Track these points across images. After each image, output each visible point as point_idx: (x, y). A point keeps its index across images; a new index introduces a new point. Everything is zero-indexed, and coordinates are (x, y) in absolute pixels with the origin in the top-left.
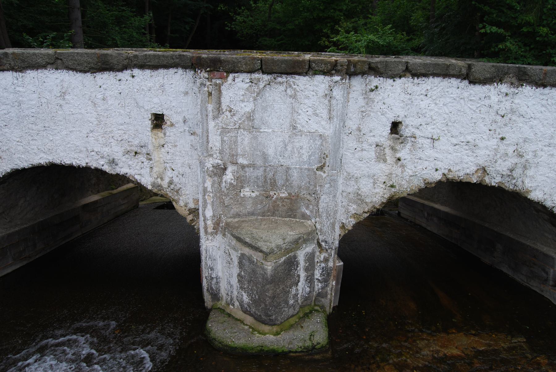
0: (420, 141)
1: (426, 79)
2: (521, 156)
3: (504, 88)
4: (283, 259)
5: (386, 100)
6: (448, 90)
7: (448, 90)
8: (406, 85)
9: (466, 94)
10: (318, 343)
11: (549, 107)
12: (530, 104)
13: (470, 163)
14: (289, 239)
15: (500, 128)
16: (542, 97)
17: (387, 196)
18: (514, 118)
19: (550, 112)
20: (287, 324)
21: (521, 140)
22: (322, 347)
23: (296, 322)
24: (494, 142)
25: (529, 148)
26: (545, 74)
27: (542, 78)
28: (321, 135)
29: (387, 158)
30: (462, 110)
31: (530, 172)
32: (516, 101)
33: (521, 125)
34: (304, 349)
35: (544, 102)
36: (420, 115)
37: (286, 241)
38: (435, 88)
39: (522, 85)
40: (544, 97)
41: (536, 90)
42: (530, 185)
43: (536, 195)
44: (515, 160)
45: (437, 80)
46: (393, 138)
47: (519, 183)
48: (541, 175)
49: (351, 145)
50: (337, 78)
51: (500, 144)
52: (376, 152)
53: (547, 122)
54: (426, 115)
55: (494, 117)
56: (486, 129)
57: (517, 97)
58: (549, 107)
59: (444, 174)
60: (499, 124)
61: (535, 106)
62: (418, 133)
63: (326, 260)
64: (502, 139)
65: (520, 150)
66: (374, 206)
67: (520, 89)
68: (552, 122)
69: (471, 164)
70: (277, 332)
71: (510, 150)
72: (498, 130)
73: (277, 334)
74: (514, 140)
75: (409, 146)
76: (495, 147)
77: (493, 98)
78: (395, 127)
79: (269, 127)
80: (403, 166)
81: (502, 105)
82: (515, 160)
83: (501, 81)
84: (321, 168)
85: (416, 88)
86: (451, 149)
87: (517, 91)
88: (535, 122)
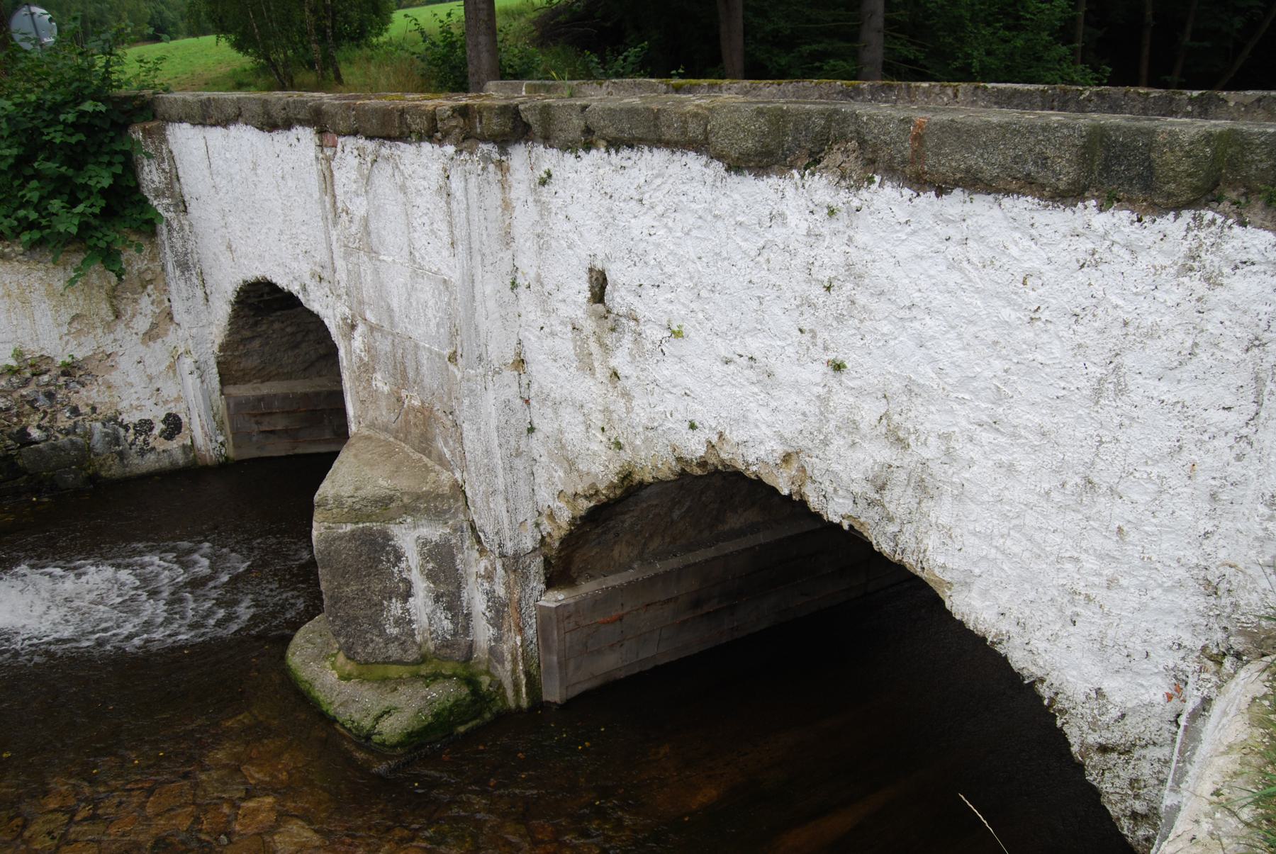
0: (648, 332)
1: (634, 155)
2: (900, 442)
3: (821, 187)
4: (349, 528)
5: (570, 208)
6: (685, 188)
7: (685, 188)
8: (601, 171)
9: (724, 205)
10: (380, 734)
11: (974, 274)
12: (902, 252)
13: (764, 427)
14: (369, 491)
15: (827, 326)
16: (943, 230)
17: (615, 467)
18: (862, 300)
19: (978, 291)
20: (379, 671)
21: (898, 385)
22: (383, 744)
23: (401, 677)
24: (816, 372)
25: (929, 420)
26: (918, 138)
27: (908, 153)
28: (445, 281)
29: (596, 364)
30: (724, 254)
31: (942, 512)
32: (861, 238)
33: (886, 328)
34: (356, 728)
35: (953, 250)
36: (636, 259)
37: (360, 493)
38: (659, 181)
39: (871, 181)
40: (951, 231)
41: (916, 201)
42: (941, 560)
43: (973, 607)
44: (885, 454)
45: (659, 157)
46: (594, 313)
47: (906, 539)
48: (975, 534)
49: (532, 316)
50: (450, 149)
51: (833, 383)
52: (574, 341)
53: (973, 329)
54: (646, 258)
55: (805, 287)
56: (788, 324)
57: (865, 218)
58: (974, 274)
59: (711, 446)
60: (821, 314)
61: (925, 264)
62: (641, 310)
63: (489, 576)
64: (838, 367)
65: (896, 418)
66: (594, 484)
67: (864, 194)
68: (992, 336)
69: (769, 433)
70: (349, 675)
71: (869, 412)
72: (823, 335)
73: (347, 678)
74: (872, 380)
75: (627, 340)
76: (820, 390)
77: (793, 219)
78: (599, 287)
79: (389, 255)
80: (626, 394)
81: (820, 250)
82: (885, 454)
83: (814, 161)
84: (453, 358)
85: (619, 180)
86: (718, 368)
87: (856, 203)
88: (933, 325)
